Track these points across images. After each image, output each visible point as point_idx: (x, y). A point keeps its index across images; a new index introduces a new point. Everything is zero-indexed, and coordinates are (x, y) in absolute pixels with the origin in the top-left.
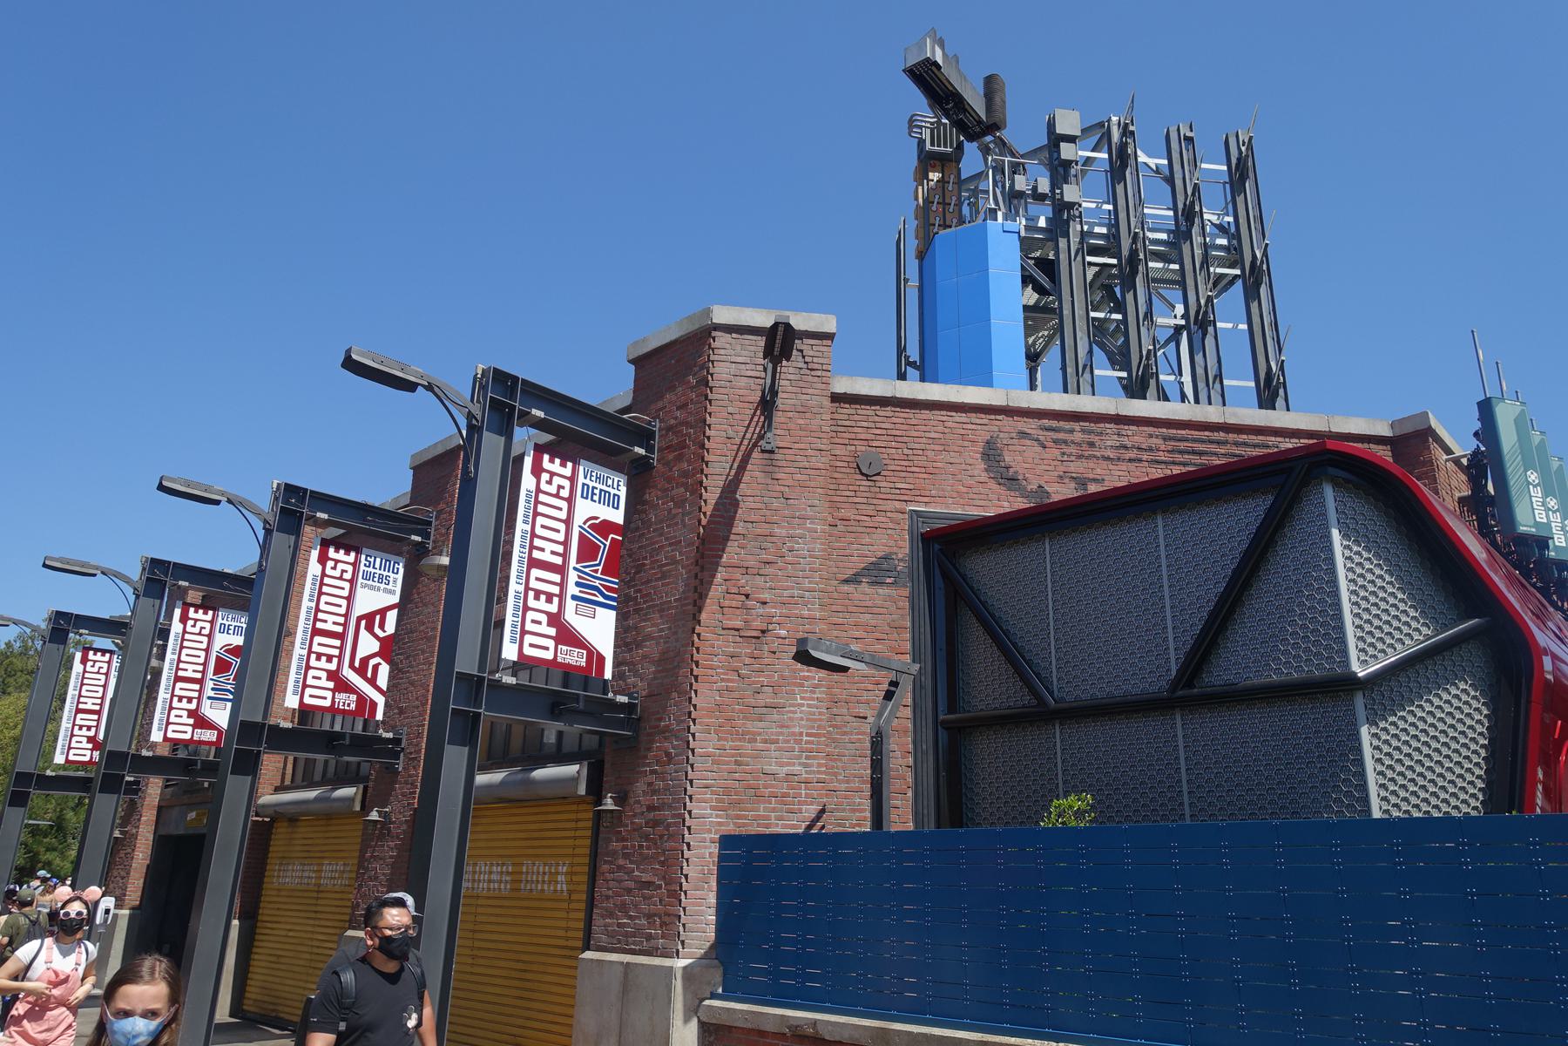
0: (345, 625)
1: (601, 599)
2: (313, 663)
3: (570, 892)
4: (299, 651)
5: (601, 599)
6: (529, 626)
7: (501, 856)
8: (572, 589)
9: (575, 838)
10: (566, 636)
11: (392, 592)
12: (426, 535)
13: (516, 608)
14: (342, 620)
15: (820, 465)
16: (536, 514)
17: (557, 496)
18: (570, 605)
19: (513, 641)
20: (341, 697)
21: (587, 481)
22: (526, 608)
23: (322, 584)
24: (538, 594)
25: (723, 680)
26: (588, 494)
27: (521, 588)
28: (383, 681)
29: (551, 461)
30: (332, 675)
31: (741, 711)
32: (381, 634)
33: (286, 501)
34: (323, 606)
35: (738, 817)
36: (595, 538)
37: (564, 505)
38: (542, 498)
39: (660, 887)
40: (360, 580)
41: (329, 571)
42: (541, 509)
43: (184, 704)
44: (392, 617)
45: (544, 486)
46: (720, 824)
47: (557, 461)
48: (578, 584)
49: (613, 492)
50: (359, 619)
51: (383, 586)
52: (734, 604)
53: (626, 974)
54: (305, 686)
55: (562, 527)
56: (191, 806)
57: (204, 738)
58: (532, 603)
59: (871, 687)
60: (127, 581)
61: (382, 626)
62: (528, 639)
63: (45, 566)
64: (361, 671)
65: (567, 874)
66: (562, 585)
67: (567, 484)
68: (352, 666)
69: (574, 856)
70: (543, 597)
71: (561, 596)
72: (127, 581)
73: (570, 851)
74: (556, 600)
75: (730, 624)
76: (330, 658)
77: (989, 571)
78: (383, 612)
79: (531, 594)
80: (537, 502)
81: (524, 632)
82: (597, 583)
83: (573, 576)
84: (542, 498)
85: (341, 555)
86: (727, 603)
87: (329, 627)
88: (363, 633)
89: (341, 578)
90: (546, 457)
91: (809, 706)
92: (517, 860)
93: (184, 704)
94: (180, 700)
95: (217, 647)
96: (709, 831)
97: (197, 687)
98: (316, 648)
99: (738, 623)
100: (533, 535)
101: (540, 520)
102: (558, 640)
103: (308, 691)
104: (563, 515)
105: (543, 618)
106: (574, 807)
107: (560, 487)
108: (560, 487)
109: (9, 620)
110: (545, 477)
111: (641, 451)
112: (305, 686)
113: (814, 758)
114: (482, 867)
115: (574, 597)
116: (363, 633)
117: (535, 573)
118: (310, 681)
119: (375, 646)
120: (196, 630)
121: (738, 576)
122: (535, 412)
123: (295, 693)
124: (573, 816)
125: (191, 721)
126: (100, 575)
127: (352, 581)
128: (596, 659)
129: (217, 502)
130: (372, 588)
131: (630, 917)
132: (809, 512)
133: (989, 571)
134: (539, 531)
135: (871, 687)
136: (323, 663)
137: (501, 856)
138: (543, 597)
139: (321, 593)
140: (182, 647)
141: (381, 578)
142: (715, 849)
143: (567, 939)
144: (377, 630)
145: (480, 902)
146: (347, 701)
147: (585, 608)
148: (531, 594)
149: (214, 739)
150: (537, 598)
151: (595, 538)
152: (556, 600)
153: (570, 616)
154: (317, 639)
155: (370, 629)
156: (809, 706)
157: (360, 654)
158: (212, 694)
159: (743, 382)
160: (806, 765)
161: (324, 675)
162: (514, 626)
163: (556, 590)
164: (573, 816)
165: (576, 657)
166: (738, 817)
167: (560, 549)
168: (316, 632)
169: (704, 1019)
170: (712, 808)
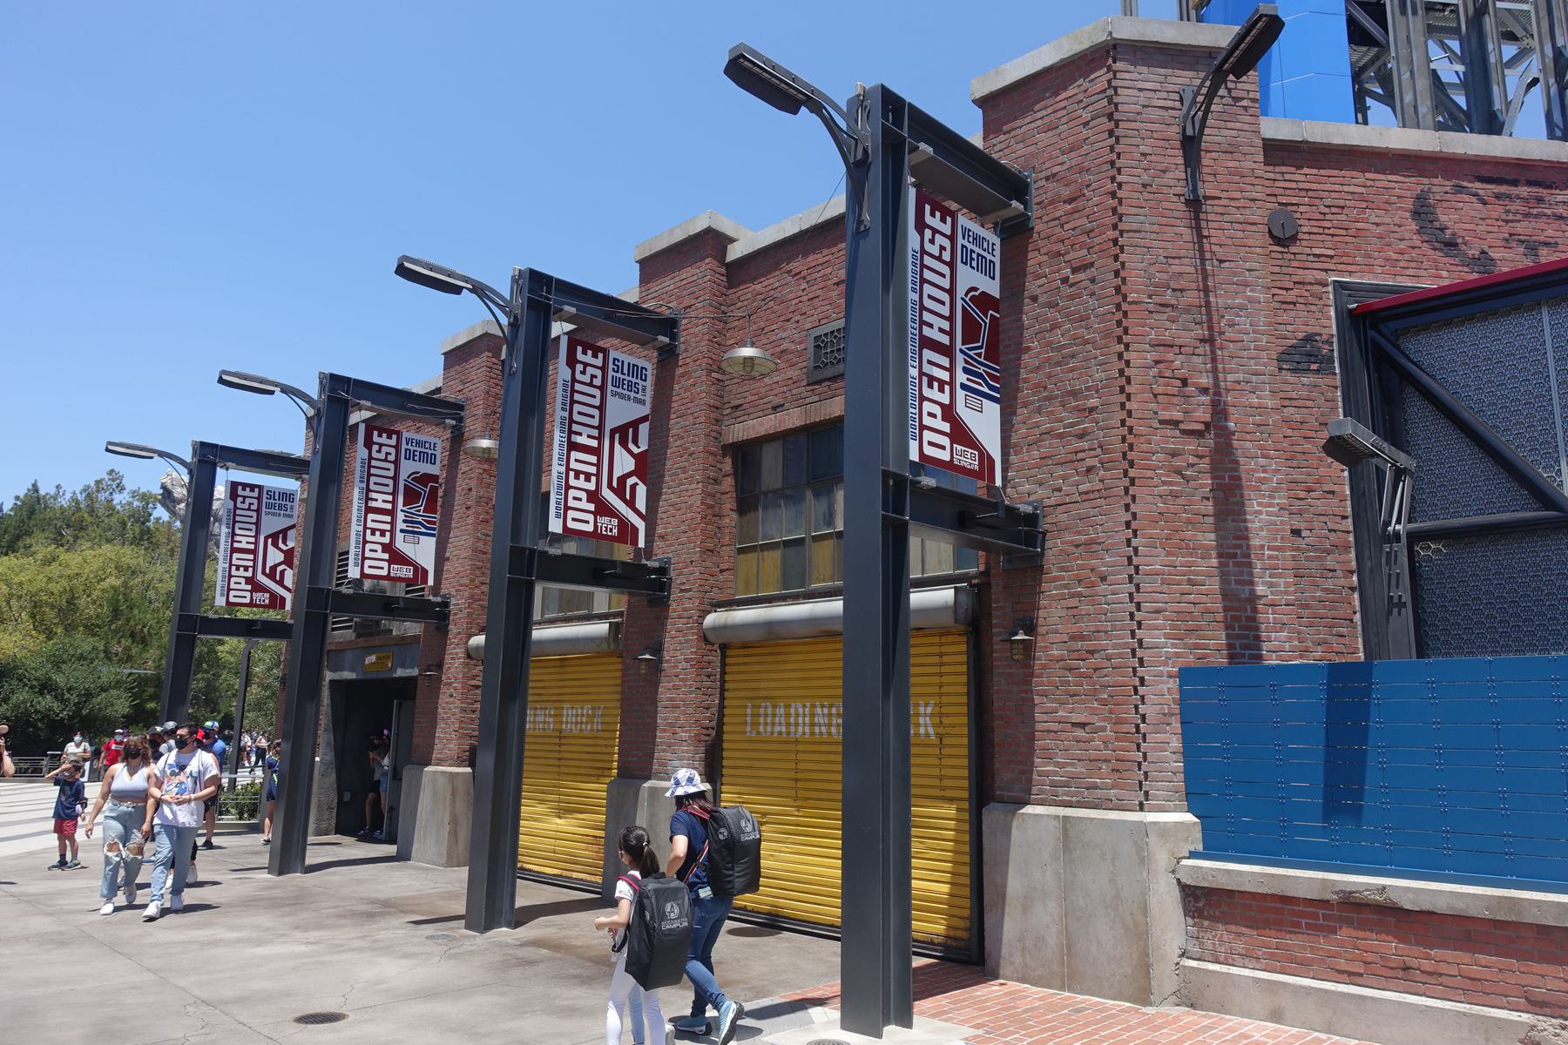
0: (256, 543)
1: (986, 390)
2: (234, 572)
3: (940, 737)
4: (355, 528)
5: (986, 390)
6: (571, 503)
7: (812, 697)
8: (400, 525)
9: (941, 675)
10: (396, 557)
11: (642, 402)
12: (673, 337)
13: (357, 542)
14: (390, 498)
15: (1255, 218)
16: (573, 402)
17: (591, 384)
18: (399, 536)
19: (356, 565)
20: (604, 521)
21: (965, 243)
22: (568, 487)
23: (370, 466)
24: (577, 474)
25: (1164, 483)
26: (410, 456)
27: (563, 469)
28: (641, 504)
29: (584, 353)
30: (249, 581)
31: (1189, 521)
32: (636, 451)
33: (332, 390)
34: (372, 487)
35: (1197, 646)
36: (975, 312)
37: (597, 393)
38: (578, 387)
39: (1103, 729)
40: (610, 388)
41: (374, 455)
42: (577, 397)
43: (377, 538)
44: (644, 429)
45: (579, 376)
46: (1177, 655)
47: (938, 214)
48: (965, 370)
49: (989, 257)
50: (613, 432)
51: (632, 395)
52: (1170, 390)
53: (1065, 830)
54: (364, 558)
55: (391, 482)
56: (369, 650)
57: (399, 574)
58: (572, 482)
59: (1302, 494)
60: (183, 462)
61: (636, 442)
62: (367, 563)
63: (221, 381)
64: (272, 576)
65: (932, 715)
66: (393, 523)
67: (599, 373)
68: (264, 572)
69: (941, 695)
70: (582, 477)
71: (392, 531)
72: (183, 462)
73: (936, 690)
74: (593, 479)
75: (1165, 415)
76: (588, 477)
77: (1445, 356)
78: (635, 424)
79: (572, 474)
80: (573, 391)
81: (567, 508)
82: (981, 370)
83: (400, 516)
84: (578, 387)
85: (384, 439)
86: (1161, 389)
87: (243, 546)
88: (270, 548)
89: (386, 460)
90: (579, 349)
91: (1268, 514)
92: (757, 702)
93: (377, 538)
94: (373, 533)
95: (403, 475)
96: (1165, 664)
97: (388, 519)
98: (370, 524)
99: (1178, 415)
100: (571, 421)
101: (577, 408)
102: (390, 562)
103: (232, 593)
104: (391, 474)
105: (583, 495)
106: (936, 639)
107: (593, 376)
108: (593, 376)
109: (276, 384)
110: (579, 367)
111: (667, 340)
112: (364, 558)
113: (1280, 576)
114: (797, 707)
115: (963, 386)
116: (270, 548)
117: (575, 455)
118: (368, 554)
119: (280, 557)
120: (382, 456)
121: (1170, 356)
122: (566, 308)
123: (558, 516)
124: (936, 649)
125: (386, 556)
126: (156, 458)
127: (258, 511)
128: (421, 573)
129: (272, 393)
130: (622, 396)
131: (1057, 764)
132: (1249, 277)
133: (1445, 356)
134: (576, 417)
135: (1302, 494)
136: (241, 572)
137: (812, 697)
138: (582, 477)
139: (369, 475)
140: (369, 475)
141: (630, 386)
142: (1174, 684)
143: (943, 788)
144: (281, 545)
145: (800, 747)
146: (609, 525)
147: (409, 537)
148: (572, 474)
149: (411, 575)
150: (577, 477)
151: (417, 487)
152: (593, 479)
153: (401, 544)
154: (236, 555)
155: (275, 545)
156: (1268, 514)
157: (270, 564)
158: (404, 526)
159: (1154, 114)
160: (1271, 585)
161: (379, 548)
162: (558, 503)
163: (593, 470)
164: (936, 649)
165: (969, 459)
166: (1197, 646)
167: (595, 433)
168: (234, 550)
169: (1187, 880)
170: (1167, 636)
